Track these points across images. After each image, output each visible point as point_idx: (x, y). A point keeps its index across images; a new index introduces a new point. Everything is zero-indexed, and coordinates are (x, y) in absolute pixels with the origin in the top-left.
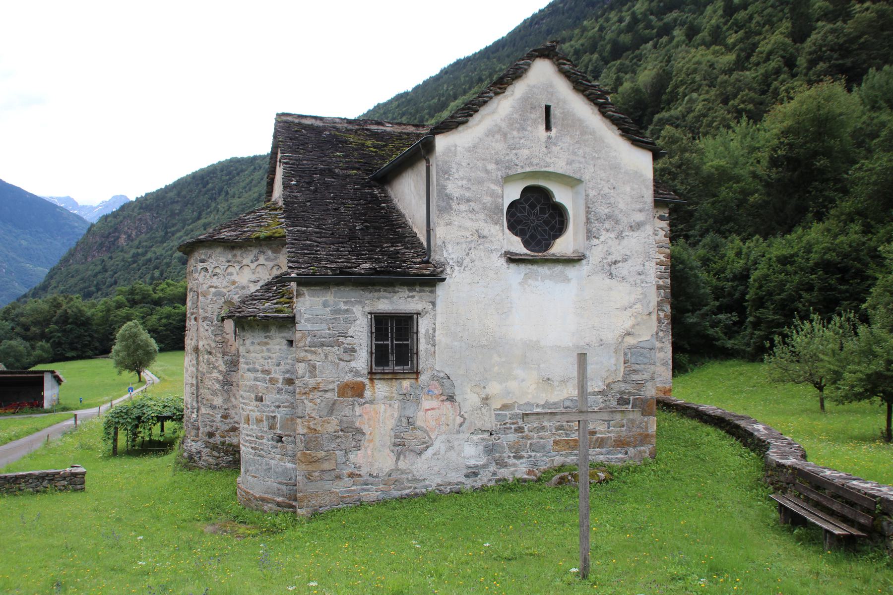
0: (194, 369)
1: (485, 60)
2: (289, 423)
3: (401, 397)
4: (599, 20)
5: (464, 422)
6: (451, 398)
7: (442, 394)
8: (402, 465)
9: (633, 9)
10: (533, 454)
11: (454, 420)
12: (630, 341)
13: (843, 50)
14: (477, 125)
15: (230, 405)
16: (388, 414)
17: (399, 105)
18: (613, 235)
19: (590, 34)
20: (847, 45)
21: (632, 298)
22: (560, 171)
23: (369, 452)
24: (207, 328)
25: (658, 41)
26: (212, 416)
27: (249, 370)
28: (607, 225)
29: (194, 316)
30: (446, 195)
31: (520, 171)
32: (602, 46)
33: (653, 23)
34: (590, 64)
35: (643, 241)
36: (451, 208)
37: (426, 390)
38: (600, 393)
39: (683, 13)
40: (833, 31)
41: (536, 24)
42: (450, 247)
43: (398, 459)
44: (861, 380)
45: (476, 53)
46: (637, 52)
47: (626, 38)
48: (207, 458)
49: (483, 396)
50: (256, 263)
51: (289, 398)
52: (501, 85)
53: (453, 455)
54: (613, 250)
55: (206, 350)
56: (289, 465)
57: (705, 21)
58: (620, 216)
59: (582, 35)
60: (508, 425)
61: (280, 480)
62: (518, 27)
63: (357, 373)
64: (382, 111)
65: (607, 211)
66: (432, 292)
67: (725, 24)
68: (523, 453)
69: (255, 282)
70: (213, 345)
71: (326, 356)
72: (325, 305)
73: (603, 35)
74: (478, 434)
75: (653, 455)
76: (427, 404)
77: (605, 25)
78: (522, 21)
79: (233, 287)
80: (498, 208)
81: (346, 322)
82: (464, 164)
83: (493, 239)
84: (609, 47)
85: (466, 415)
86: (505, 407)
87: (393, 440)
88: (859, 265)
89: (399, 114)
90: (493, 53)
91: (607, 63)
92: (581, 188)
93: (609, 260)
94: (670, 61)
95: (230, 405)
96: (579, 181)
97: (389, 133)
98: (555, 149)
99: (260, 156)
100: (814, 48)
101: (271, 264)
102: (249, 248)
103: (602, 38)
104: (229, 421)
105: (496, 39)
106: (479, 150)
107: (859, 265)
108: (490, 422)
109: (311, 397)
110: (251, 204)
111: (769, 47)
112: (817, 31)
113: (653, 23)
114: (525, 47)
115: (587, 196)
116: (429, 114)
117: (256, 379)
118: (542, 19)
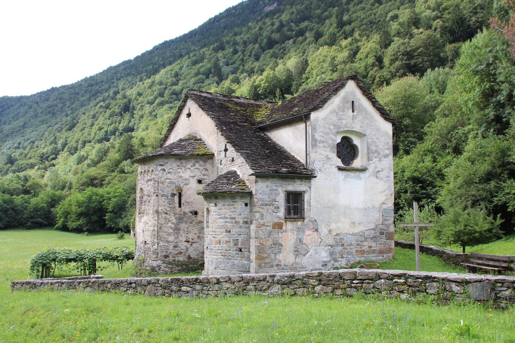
0: (156, 222)
1: (183, 42)
2: (246, 242)
3: (297, 229)
4: (259, 23)
5: (321, 241)
6: (317, 230)
7: (313, 228)
8: (298, 260)
9: (280, 18)
10: (348, 256)
11: (318, 240)
12: (384, 206)
13: (409, 55)
14: (326, 108)
15: (178, 240)
16: (292, 237)
17: (125, 69)
18: (377, 160)
19: (253, 31)
20: (411, 52)
21: (385, 187)
22: (357, 130)
23: (285, 254)
24: (164, 200)
25: (296, 39)
26: (167, 246)
27: (220, 218)
28: (375, 155)
29: (156, 194)
30: (315, 139)
31: (343, 130)
32: (261, 39)
33: (293, 28)
34: (253, 50)
35: (389, 162)
36: (317, 145)
37: (307, 226)
38: (373, 229)
39: (311, 23)
40: (403, 44)
41: (216, 22)
42: (316, 162)
43: (296, 258)
44: (452, 235)
45: (177, 38)
46: (283, 45)
47: (276, 36)
48: (165, 269)
49: (329, 229)
50: (194, 167)
51: (246, 230)
52: (336, 91)
53: (317, 256)
54: (377, 166)
55: (164, 212)
56: (245, 262)
57: (326, 29)
58: (380, 151)
59: (248, 32)
60: (338, 243)
61: (240, 269)
62: (205, 23)
63: (280, 218)
64: (113, 72)
65: (375, 149)
66: (310, 182)
67: (339, 32)
68: (344, 256)
69: (193, 177)
70: (168, 209)
71: (268, 210)
72: (267, 187)
73: (262, 32)
74: (327, 247)
75: (394, 258)
76: (308, 232)
77: (263, 26)
78: (208, 19)
79: (180, 179)
80: (334, 146)
81: (276, 195)
82: (322, 126)
83: (333, 160)
84: (265, 41)
85: (322, 238)
86: (337, 235)
87: (294, 249)
88: (431, 179)
89: (125, 74)
90: (188, 38)
91: (264, 51)
92: (364, 138)
93: (376, 171)
94: (305, 53)
95: (178, 240)
96: (365, 135)
97: (243, 103)
98: (356, 120)
99: (25, 97)
100: (393, 53)
101: (202, 168)
102: (190, 159)
103: (260, 35)
104: (177, 249)
105: (191, 30)
106: (327, 120)
107: (431, 179)
108: (332, 242)
109: (261, 229)
110: (18, 129)
111: (367, 50)
112: (394, 43)
113: (293, 28)
114: (210, 36)
115: (368, 142)
116: (146, 76)
117: (226, 222)
118: (221, 19)
